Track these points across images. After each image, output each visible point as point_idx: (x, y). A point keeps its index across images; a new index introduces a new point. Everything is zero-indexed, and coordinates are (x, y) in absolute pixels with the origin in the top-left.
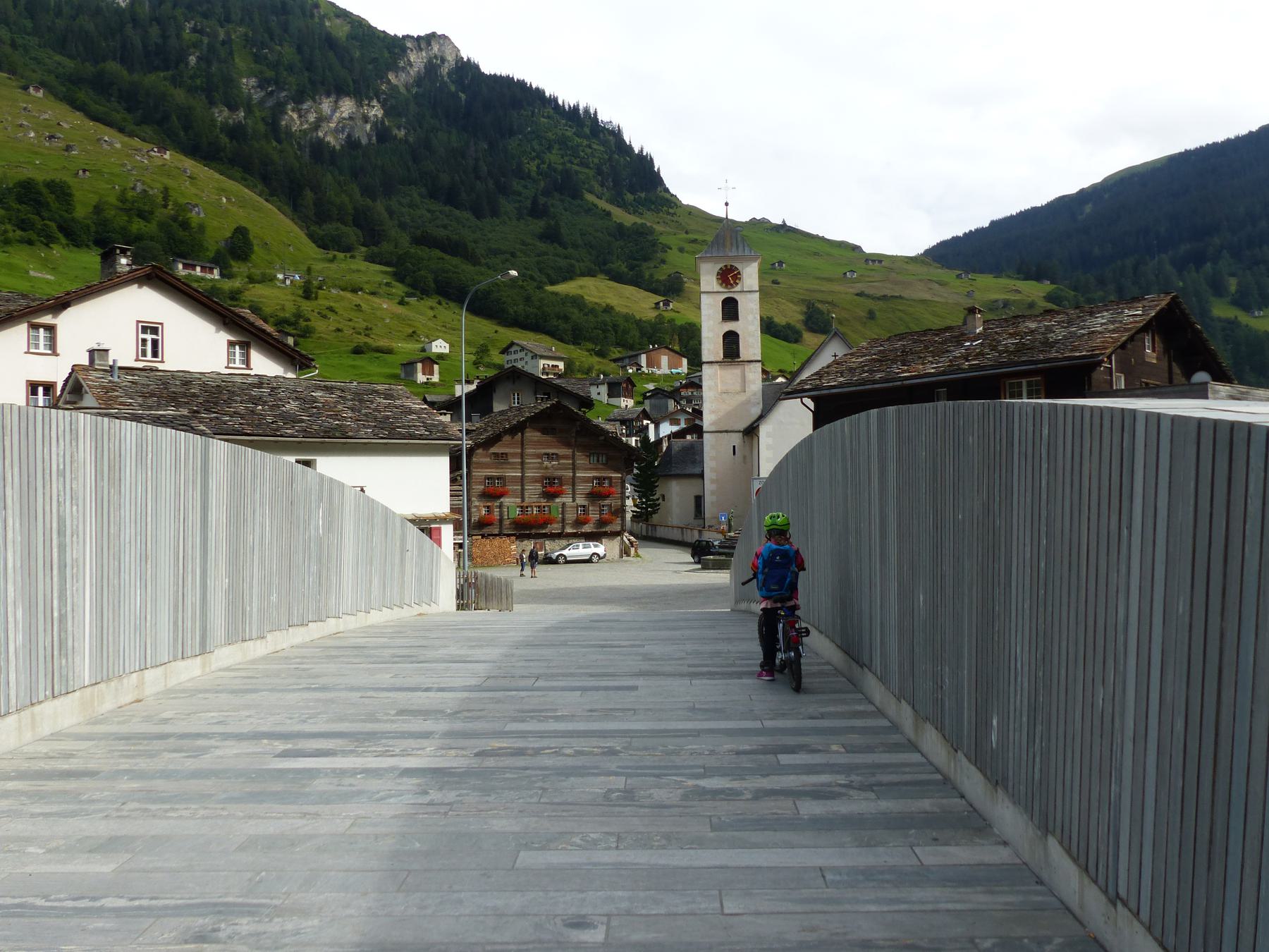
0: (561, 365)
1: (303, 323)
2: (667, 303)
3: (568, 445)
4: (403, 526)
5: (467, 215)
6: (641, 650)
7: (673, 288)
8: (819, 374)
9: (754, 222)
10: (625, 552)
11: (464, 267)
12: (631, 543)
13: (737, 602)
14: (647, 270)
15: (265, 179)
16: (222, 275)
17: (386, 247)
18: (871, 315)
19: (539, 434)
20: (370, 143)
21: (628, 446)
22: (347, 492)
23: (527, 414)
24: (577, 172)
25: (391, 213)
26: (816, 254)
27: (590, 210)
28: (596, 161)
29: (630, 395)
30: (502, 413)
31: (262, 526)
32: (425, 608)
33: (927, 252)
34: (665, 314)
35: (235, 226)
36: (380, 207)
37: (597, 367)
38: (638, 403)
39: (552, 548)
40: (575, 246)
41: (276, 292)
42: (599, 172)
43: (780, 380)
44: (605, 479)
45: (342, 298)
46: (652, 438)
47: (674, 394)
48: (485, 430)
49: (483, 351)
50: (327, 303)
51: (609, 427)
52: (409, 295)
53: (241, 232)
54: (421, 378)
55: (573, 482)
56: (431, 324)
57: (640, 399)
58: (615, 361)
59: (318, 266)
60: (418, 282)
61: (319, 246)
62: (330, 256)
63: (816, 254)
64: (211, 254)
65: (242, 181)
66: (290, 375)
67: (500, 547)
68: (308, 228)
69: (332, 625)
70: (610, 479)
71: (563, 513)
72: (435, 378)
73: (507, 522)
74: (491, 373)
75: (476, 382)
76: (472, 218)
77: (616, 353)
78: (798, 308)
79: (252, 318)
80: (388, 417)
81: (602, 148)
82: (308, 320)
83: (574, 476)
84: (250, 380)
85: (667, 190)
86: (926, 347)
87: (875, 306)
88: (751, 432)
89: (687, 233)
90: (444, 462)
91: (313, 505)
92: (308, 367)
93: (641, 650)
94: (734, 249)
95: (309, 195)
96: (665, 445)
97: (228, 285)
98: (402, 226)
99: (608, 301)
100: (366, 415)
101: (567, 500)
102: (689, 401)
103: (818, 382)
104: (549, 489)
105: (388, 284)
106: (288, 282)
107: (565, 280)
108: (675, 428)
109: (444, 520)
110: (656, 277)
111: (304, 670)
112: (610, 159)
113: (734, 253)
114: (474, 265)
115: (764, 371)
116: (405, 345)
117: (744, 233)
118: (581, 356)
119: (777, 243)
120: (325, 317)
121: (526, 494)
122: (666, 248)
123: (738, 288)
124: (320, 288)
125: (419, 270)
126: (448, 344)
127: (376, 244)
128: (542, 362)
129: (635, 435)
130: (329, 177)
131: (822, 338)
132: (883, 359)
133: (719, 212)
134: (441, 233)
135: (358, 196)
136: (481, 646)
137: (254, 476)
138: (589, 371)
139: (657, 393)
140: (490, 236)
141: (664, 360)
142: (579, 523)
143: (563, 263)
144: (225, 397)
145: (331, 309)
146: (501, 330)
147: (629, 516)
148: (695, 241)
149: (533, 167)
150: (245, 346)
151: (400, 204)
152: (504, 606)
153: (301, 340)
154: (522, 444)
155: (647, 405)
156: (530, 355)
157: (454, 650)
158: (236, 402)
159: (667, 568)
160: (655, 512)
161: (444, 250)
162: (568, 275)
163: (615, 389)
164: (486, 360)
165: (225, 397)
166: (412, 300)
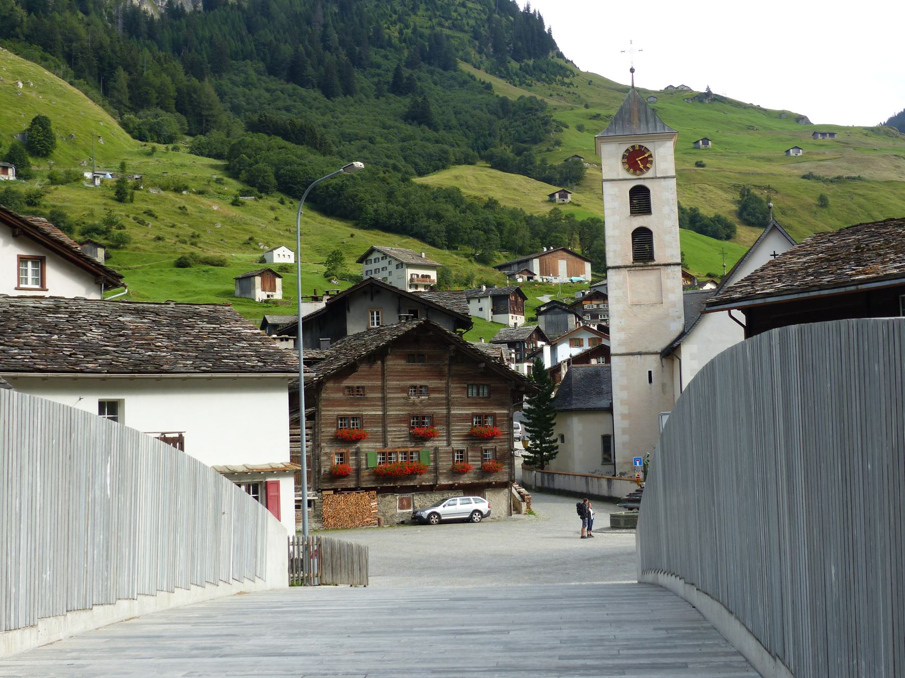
0: (433, 275)
1: (115, 232)
2: (564, 195)
3: (440, 375)
4: (217, 483)
5: (315, 94)
6: (504, 638)
7: (571, 176)
8: (751, 280)
9: (672, 93)
10: (514, 508)
11: (312, 157)
12: (522, 497)
13: (644, 572)
14: (537, 154)
15: (70, 59)
16: (18, 175)
17: (216, 136)
18: (823, 202)
19: (403, 362)
20: (195, 11)
21: (515, 376)
22: (142, 442)
23: (388, 338)
24: (448, 37)
25: (221, 95)
26: (750, 128)
27: (465, 82)
28: (472, 22)
29: (519, 309)
30: (357, 336)
31: (32, 486)
32: (247, 585)
33: (892, 121)
34: (563, 208)
35: (33, 116)
36: (208, 87)
37: (478, 276)
38: (531, 320)
39: (424, 504)
40: (448, 128)
41: (83, 193)
42: (476, 36)
43: (709, 287)
44: (486, 416)
45: (163, 200)
46: (547, 364)
47: (575, 308)
48: (337, 358)
49: (335, 259)
50: (145, 206)
51: (492, 352)
52: (245, 193)
53: (41, 123)
54: (260, 295)
55: (448, 420)
56: (271, 228)
57: (533, 315)
58: (500, 268)
59: (134, 162)
60: (253, 178)
61: (134, 137)
62: (148, 149)
63: (750, 128)
64: (5, 151)
65: (42, 61)
66: (94, 296)
67: (357, 504)
68: (121, 115)
69: (123, 609)
70: (494, 416)
71: (435, 460)
72: (278, 295)
73: (365, 473)
74: (346, 286)
75: (326, 298)
76: (322, 98)
77: (501, 258)
78: (729, 196)
79: (49, 228)
80: (212, 346)
81: (479, 7)
82: (121, 227)
83: (449, 413)
84: (44, 304)
85: (561, 55)
86: (887, 242)
87: (828, 190)
88: (671, 353)
89: (587, 107)
90: (282, 399)
91: (98, 460)
92: (116, 286)
93: (504, 638)
94: (643, 126)
95: (122, 77)
96: (564, 372)
97: (25, 187)
98: (236, 109)
99: (491, 194)
100: (185, 343)
101: (441, 444)
102: (594, 316)
103: (749, 289)
104: (417, 430)
105: (219, 181)
106: (98, 182)
107: (436, 169)
108: (576, 351)
109: (282, 472)
110: (549, 163)
111: (79, 666)
112: (489, 20)
113: (643, 130)
114: (324, 154)
115: (685, 275)
116: (240, 255)
117: (659, 104)
118: (458, 263)
119: (701, 114)
120: (142, 223)
121: (389, 438)
122: (561, 126)
123: (649, 174)
124: (136, 188)
125: (257, 163)
126: (292, 257)
127: (203, 133)
128: (410, 272)
129: (527, 360)
130: (147, 54)
131: (759, 231)
132: (833, 258)
133: (625, 80)
134: (283, 117)
135: (181, 76)
136: (304, 634)
137: (21, 425)
138: (468, 281)
139: (554, 306)
140: (343, 118)
141: (562, 265)
142: (456, 472)
143: (432, 148)
144: (14, 325)
145: (149, 213)
146: (358, 233)
147: (519, 463)
148: (597, 117)
149: (393, 32)
150: (39, 262)
151: (234, 83)
152: (357, 580)
153: (113, 252)
154: (383, 374)
155: (541, 323)
156: (394, 263)
157: (270, 640)
158: (27, 330)
159: (553, 528)
160: (551, 457)
161: (286, 137)
162: (440, 163)
163: (500, 303)
164: (340, 270)
165: (14, 325)
166: (248, 200)
